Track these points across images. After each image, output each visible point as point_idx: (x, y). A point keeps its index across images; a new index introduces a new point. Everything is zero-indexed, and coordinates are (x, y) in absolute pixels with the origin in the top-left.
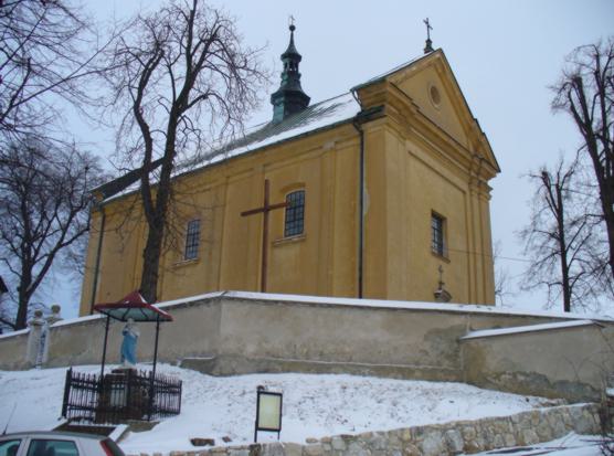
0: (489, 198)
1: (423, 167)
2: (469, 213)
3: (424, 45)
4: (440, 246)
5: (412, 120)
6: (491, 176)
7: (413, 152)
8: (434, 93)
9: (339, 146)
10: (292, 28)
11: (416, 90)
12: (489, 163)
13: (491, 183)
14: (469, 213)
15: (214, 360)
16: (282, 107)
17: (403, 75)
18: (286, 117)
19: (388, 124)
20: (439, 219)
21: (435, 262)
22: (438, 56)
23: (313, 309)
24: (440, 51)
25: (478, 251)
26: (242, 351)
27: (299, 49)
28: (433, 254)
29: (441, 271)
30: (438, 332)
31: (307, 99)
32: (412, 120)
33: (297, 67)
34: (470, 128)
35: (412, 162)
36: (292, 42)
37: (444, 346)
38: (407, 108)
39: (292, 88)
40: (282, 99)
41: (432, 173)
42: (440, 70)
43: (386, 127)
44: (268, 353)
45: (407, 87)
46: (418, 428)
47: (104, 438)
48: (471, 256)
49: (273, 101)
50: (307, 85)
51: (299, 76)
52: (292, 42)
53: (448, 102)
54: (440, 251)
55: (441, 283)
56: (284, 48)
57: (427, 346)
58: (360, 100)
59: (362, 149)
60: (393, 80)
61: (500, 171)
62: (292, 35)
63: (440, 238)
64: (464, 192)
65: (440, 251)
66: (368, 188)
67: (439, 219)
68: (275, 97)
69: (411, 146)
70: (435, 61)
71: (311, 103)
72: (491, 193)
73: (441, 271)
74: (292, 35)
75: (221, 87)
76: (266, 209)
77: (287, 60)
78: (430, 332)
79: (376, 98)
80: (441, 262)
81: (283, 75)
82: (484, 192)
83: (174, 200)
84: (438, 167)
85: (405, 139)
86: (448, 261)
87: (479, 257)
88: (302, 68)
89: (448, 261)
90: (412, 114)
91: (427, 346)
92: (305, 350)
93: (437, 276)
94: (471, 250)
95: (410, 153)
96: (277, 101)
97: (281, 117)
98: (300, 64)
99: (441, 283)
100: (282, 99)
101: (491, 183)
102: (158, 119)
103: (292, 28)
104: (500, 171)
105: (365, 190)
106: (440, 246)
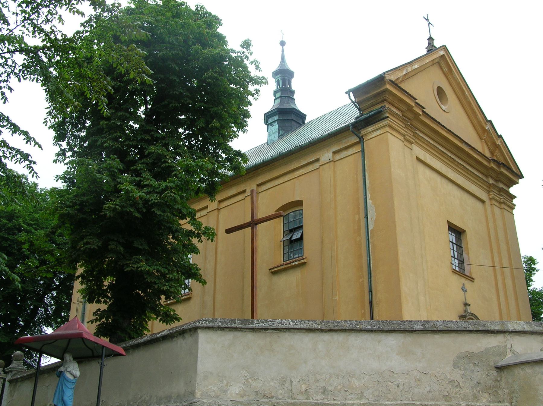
0: (513, 207)
1: (434, 175)
2: (491, 225)
3: (427, 44)
4: (461, 262)
5: (419, 125)
6: (514, 183)
7: (422, 158)
8: (440, 92)
9: (338, 157)
10: (283, 43)
11: (422, 91)
12: (509, 169)
13: (513, 190)
14: (491, 225)
15: (157, 398)
16: (276, 126)
17: (404, 72)
18: (280, 137)
19: (390, 126)
20: (457, 232)
21: (456, 281)
22: (442, 53)
23: (311, 335)
24: (444, 48)
25: (506, 263)
26: (225, 392)
27: (291, 65)
28: (454, 271)
30: (469, 356)
31: (303, 117)
32: (419, 125)
33: (290, 83)
34: (484, 130)
35: (421, 168)
37: (480, 375)
39: (286, 106)
40: (276, 118)
41: (444, 181)
42: (446, 69)
43: (387, 129)
44: (257, 393)
45: (409, 87)
46: (533, 315)
48: (498, 269)
49: (266, 122)
50: (301, 103)
51: (293, 93)
53: (456, 101)
55: (466, 305)
57: (457, 375)
58: (359, 105)
59: (363, 156)
60: (393, 78)
61: (521, 177)
62: (283, 51)
63: (460, 254)
64: (483, 202)
66: (371, 199)
67: (457, 232)
68: (268, 116)
69: (419, 151)
70: (440, 60)
71: (307, 121)
72: (515, 201)
74: (283, 51)
76: (254, 223)
77: (279, 77)
78: (460, 357)
79: (378, 101)
80: (463, 280)
81: (275, 92)
82: (507, 202)
84: (451, 174)
85: (412, 143)
86: (472, 279)
87: (507, 271)
88: (295, 85)
89: (472, 279)
90: (416, 115)
91: (457, 375)
92: (304, 387)
93: (460, 296)
94: (497, 265)
95: (418, 159)
96: (270, 121)
97: (275, 137)
98: (293, 80)
99: (466, 305)
100: (276, 118)
101: (513, 190)
103: (283, 43)
104: (521, 177)
105: (369, 202)
106: (461, 262)
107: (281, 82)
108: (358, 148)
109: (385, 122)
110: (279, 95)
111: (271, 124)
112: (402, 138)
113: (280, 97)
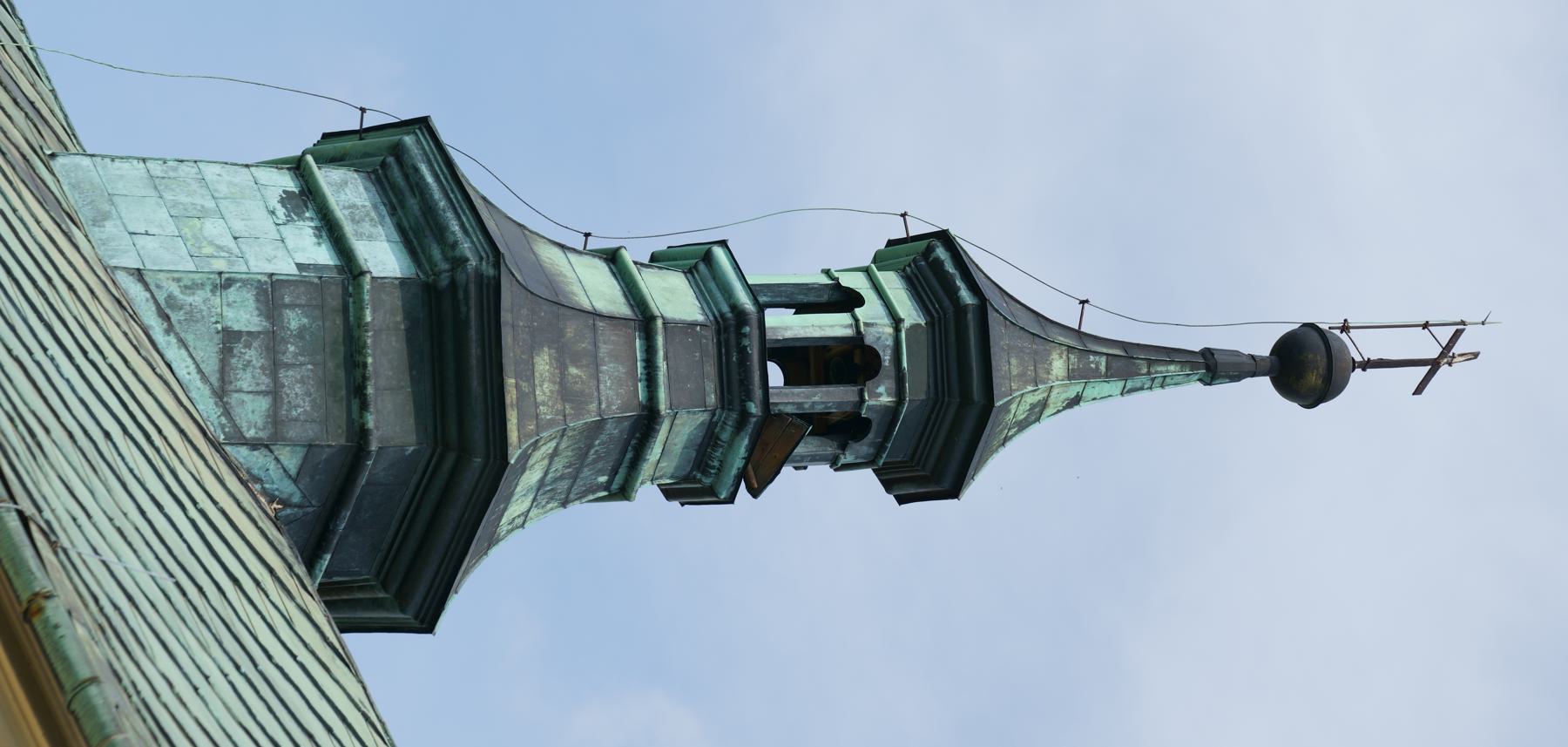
10: (1307, 366)
36: (1134, 364)
52: (1134, 364)
62: (1214, 367)
100: (382, 257)
107: (833, 325)
110: (673, 297)
111: (307, 198)
113: (644, 319)
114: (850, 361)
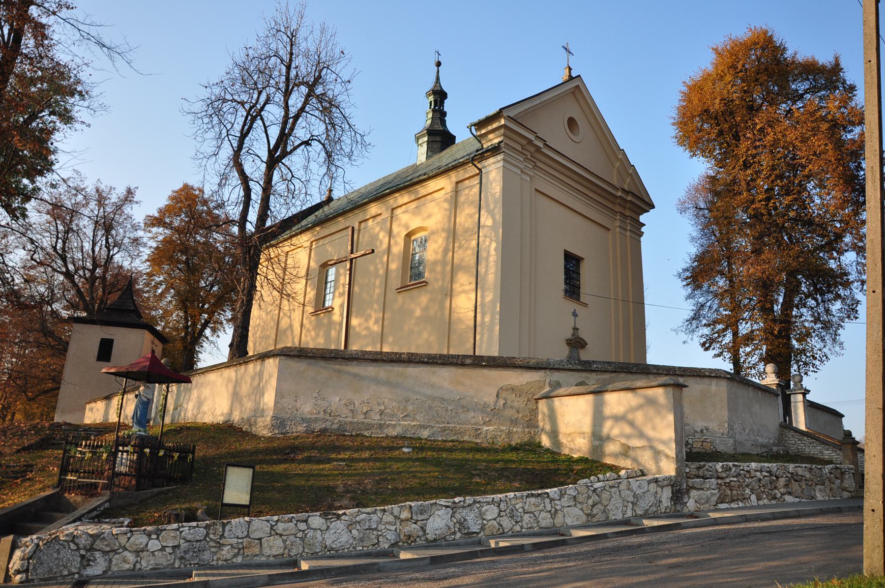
10: (439, 64)
13: (643, 218)
29: (575, 314)
36: (438, 79)
38: (530, 142)
47: (679, 507)
52: (438, 79)
54: (573, 289)
56: (430, 85)
60: (512, 113)
65: (573, 289)
72: (643, 229)
73: (575, 314)
75: (319, 128)
82: (637, 229)
83: (214, 257)
90: (538, 149)
101: (643, 218)
102: (255, 168)
103: (439, 64)
104: (653, 207)
108: (476, 181)
109: (500, 157)
112: (519, 172)
114: (435, 101)
